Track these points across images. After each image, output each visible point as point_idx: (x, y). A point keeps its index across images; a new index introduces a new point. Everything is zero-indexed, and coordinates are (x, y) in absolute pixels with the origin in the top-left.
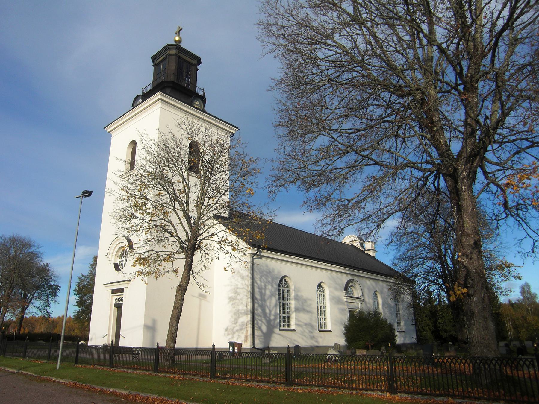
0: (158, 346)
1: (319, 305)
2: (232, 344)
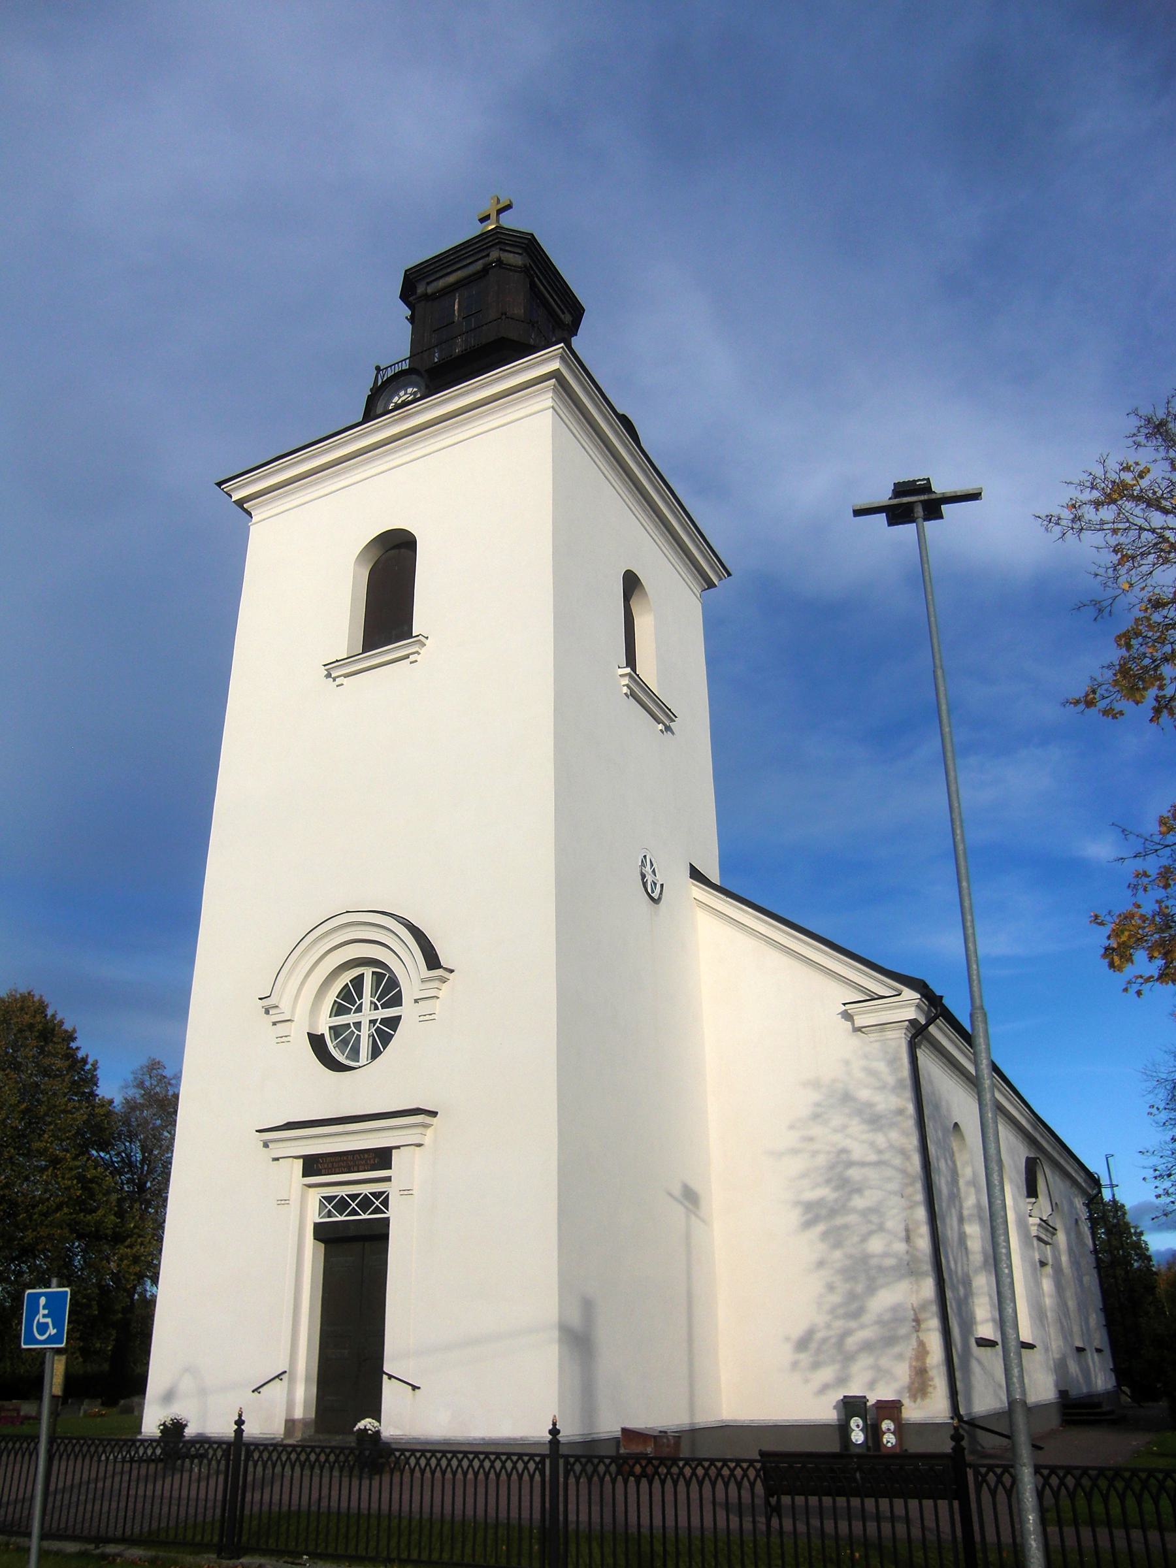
0: (239, 1432)
2: (852, 1406)
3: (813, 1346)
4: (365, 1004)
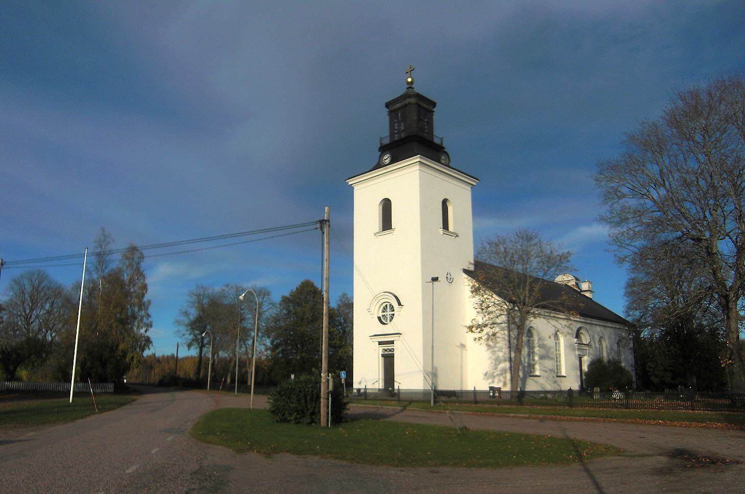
1: (556, 352)
2: (491, 388)
3: (487, 375)
4: (386, 315)
